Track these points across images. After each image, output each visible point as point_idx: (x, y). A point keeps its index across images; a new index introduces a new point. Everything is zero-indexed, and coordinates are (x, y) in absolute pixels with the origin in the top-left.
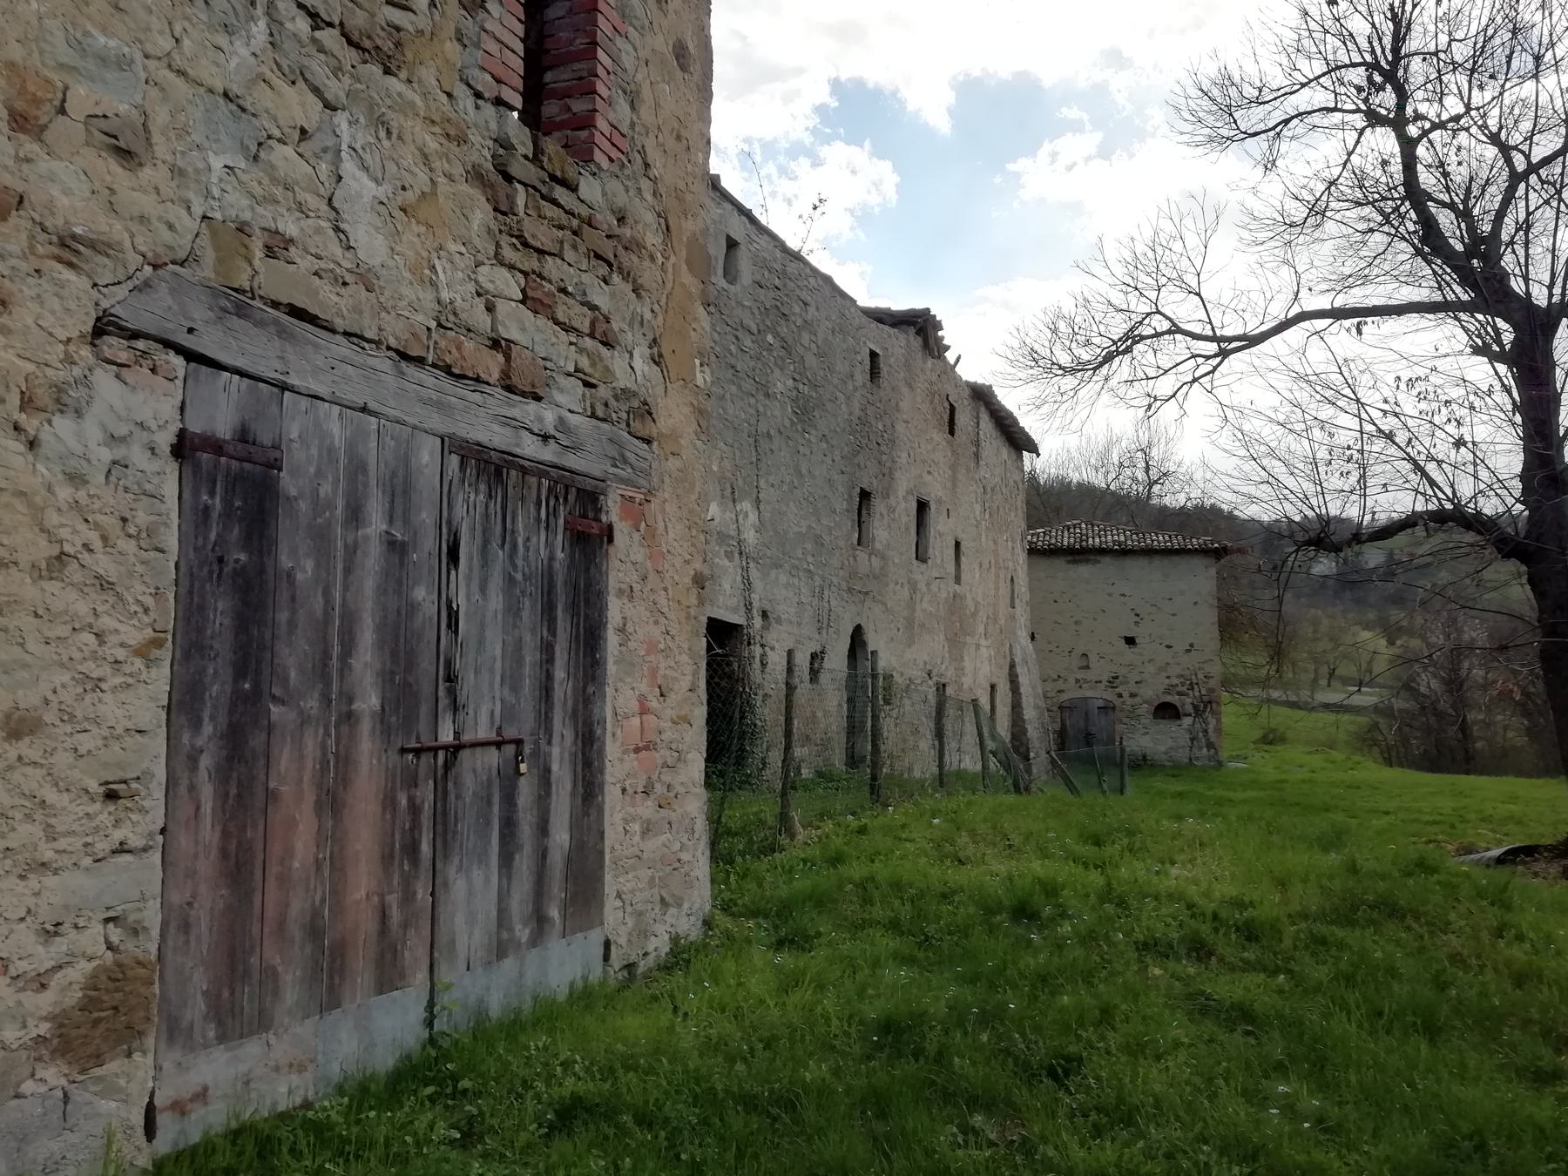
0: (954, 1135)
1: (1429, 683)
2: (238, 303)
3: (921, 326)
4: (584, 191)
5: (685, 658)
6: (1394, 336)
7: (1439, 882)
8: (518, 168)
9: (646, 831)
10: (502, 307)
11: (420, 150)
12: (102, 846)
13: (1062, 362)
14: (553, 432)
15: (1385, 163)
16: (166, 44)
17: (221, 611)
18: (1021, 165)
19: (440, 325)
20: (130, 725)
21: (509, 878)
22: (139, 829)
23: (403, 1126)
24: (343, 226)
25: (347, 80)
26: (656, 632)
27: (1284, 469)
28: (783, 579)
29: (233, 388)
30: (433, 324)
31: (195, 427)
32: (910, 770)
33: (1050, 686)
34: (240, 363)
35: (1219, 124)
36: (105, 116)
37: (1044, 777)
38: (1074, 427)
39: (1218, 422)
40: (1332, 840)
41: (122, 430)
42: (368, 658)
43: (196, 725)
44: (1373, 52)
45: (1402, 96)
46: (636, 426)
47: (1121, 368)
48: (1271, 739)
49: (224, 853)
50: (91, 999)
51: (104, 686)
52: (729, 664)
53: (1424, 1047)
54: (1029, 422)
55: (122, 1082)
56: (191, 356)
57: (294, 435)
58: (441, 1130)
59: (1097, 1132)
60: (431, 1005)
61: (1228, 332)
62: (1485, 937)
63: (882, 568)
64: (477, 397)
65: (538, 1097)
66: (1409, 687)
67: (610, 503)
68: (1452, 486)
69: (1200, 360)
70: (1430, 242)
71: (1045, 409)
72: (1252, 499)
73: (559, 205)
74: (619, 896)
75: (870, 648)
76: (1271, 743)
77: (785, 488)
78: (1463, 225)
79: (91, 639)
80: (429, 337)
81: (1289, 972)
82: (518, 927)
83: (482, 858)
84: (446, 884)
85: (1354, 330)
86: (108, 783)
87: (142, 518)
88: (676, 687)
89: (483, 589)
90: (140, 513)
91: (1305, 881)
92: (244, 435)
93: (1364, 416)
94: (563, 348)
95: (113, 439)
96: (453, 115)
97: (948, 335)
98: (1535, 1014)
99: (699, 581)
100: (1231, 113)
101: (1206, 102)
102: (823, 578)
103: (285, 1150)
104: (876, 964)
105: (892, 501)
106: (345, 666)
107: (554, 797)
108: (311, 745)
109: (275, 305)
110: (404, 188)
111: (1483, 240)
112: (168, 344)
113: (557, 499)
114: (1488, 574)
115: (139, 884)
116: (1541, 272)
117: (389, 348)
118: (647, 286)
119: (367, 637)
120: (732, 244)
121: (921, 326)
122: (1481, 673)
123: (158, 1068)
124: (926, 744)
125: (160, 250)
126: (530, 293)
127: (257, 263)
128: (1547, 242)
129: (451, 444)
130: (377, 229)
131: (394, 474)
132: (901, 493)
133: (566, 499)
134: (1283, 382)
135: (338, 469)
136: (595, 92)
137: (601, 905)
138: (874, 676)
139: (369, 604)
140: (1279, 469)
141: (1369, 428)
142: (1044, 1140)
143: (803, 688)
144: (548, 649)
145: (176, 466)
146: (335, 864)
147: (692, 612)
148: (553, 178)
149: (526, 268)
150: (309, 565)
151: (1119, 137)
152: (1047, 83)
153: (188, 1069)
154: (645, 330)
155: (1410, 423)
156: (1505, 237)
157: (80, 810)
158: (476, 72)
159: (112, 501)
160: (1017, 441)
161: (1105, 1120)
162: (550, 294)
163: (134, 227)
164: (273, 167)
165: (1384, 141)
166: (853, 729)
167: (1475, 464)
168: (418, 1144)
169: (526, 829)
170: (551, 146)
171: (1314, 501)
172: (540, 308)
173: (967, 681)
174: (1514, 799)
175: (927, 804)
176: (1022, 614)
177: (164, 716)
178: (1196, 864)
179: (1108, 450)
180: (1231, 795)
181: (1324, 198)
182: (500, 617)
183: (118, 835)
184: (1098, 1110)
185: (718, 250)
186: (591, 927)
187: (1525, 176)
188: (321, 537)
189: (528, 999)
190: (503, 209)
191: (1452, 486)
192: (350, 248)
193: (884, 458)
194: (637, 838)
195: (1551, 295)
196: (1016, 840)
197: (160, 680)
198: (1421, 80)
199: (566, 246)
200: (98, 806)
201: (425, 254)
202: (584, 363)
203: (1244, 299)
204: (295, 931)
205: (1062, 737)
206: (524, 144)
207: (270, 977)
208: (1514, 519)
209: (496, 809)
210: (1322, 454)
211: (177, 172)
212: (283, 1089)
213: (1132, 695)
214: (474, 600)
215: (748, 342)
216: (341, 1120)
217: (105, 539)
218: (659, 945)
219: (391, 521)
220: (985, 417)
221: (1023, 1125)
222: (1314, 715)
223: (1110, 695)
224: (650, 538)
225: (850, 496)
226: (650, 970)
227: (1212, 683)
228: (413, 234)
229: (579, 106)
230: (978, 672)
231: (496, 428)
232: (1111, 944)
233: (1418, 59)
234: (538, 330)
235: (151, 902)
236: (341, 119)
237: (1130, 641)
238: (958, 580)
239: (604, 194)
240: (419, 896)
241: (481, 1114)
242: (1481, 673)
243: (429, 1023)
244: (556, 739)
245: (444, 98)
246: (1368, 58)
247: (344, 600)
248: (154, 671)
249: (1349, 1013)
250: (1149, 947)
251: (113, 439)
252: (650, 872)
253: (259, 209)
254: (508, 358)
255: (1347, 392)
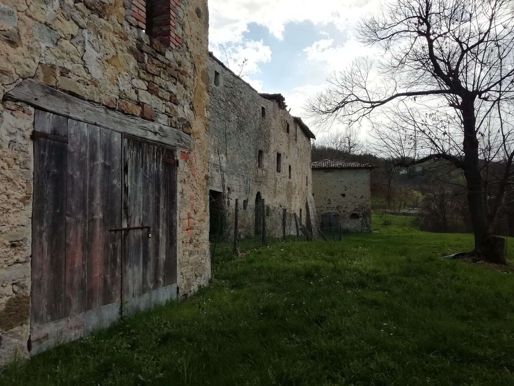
0: (287, 341)
1: (434, 206)
2: (52, 91)
3: (278, 99)
4: (167, 55)
5: (202, 201)
6: (425, 101)
7: (435, 264)
8: (144, 48)
9: (191, 254)
10: (141, 92)
11: (112, 42)
12: (11, 261)
13: (322, 110)
14: (158, 131)
15: (423, 47)
16: (25, 7)
17: (49, 189)
18: (308, 49)
19: (120, 98)
20: (19, 223)
21: (146, 269)
22: (23, 256)
23: (112, 344)
24: (86, 66)
25: (86, 19)
26: (193, 194)
27: (391, 142)
28: (235, 178)
29: (51, 118)
30: (118, 98)
31: (38, 129)
32: (275, 235)
33: (318, 209)
34: (53, 109)
35: (372, 36)
36: (5, 30)
37: (316, 236)
38: (326, 130)
39: (371, 128)
40: (403, 253)
41: (14, 131)
42: (99, 202)
43: (41, 223)
44: (420, 13)
45: (429, 27)
46: (186, 129)
47: (341, 112)
48: (386, 224)
49: (52, 263)
50: (8, 308)
51: (10, 211)
52: (217, 204)
53: (429, 311)
54: (312, 129)
55: (20, 333)
56: (36, 107)
57: (72, 132)
58: (125, 345)
59: (330, 338)
60: (121, 308)
61: (374, 100)
62: (448, 279)
63: (266, 174)
64: (133, 120)
65: (156, 334)
66: (428, 207)
67: (177, 154)
68: (442, 146)
69: (366, 109)
70: (437, 72)
71: (317, 125)
72: (381, 151)
73: (159, 60)
74: (182, 274)
75: (262, 198)
76: (386, 225)
77: (235, 150)
78: (447, 67)
79: (5, 197)
80: (117, 101)
81: (389, 291)
82: (149, 284)
83: (137, 264)
84: (125, 271)
85: (413, 99)
86: (12, 242)
87: (21, 159)
88: (200, 210)
89: (136, 180)
90: (20, 157)
91: (395, 264)
92: (55, 132)
93: (416, 125)
94: (161, 105)
95: (10, 134)
96: (123, 31)
97: (287, 102)
98: (462, 301)
99: (207, 178)
100: (374, 33)
101: (368, 29)
102: (247, 177)
103: (74, 352)
104: (263, 292)
105: (269, 154)
106: (91, 205)
107: (160, 244)
108: (80, 229)
109: (64, 91)
110: (107, 54)
111: (453, 71)
112: (28, 104)
113: (160, 152)
114: (453, 173)
115: (24, 273)
116: (470, 81)
117: (103, 105)
118: (188, 85)
119: (98, 195)
120: (217, 74)
121: (278, 99)
122: (450, 203)
123: (31, 329)
124: (280, 227)
125: (25, 73)
126: (150, 88)
127: (58, 78)
128: (473, 72)
129: (124, 135)
130: (98, 67)
131: (106, 144)
132: (272, 151)
133: (163, 153)
134: (391, 115)
135: (87, 143)
136: (170, 24)
137: (176, 277)
138: (264, 207)
139: (98, 185)
140: (390, 142)
141: (417, 129)
142: (314, 341)
143: (241, 212)
144: (157, 199)
145: (32, 142)
146: (89, 266)
147: (205, 187)
148: (157, 51)
149: (148, 79)
150: (78, 173)
151: (338, 38)
152: (315, 24)
153: (41, 329)
154: (188, 99)
155: (430, 127)
156: (460, 70)
157: (3, 250)
158: (130, 17)
159: (11, 153)
160: (309, 135)
161: (332, 335)
162: (156, 88)
163: (16, 66)
164: (62, 47)
165: (424, 41)
166: (257, 222)
167: (449, 140)
168: (117, 349)
169: (151, 254)
170: (156, 41)
171: (400, 152)
172: (153, 92)
173: (293, 208)
174: (458, 239)
175: (280, 245)
176: (310, 188)
177: (31, 221)
178: (363, 260)
179: (337, 137)
180: (374, 240)
181: (404, 59)
182: (142, 189)
183: (16, 258)
184: (330, 332)
185: (212, 76)
186: (173, 283)
187: (466, 51)
188: (82, 165)
189: (153, 305)
190: (140, 61)
191: (442, 146)
192: (89, 73)
193: (267, 140)
194: (187, 256)
195: (473, 88)
196: (307, 254)
197: (29, 209)
198: (435, 21)
199: (161, 73)
200: (9, 249)
201: (114, 75)
202: (168, 110)
203: (379, 90)
204: (76, 286)
205: (322, 225)
206: (147, 41)
207: (68, 301)
208: (461, 157)
209: (141, 248)
210: (403, 137)
211: (30, 49)
212: (73, 334)
213: (344, 212)
214: (133, 184)
215: (222, 104)
216: (92, 343)
217: (9, 165)
218: (195, 288)
219: (105, 160)
220: (298, 127)
221: (308, 337)
222: (399, 216)
223: (337, 212)
224: (191, 165)
225: (256, 152)
226: (192, 296)
227: (368, 207)
228: (110, 69)
229: (165, 29)
230: (296, 205)
231: (139, 130)
232: (335, 284)
233: (434, 15)
234: (153, 99)
235: (28, 278)
236: (85, 32)
237: (343, 195)
238: (290, 178)
239: (174, 57)
240: (117, 275)
241: (138, 339)
242: (450, 203)
243: (121, 313)
244: (161, 226)
245: (119, 26)
246: (418, 15)
247: (90, 184)
248: (27, 207)
249: (407, 302)
250: (348, 285)
251: (10, 134)
252: (191, 267)
253: (58, 61)
254: (143, 108)
255: (411, 118)
